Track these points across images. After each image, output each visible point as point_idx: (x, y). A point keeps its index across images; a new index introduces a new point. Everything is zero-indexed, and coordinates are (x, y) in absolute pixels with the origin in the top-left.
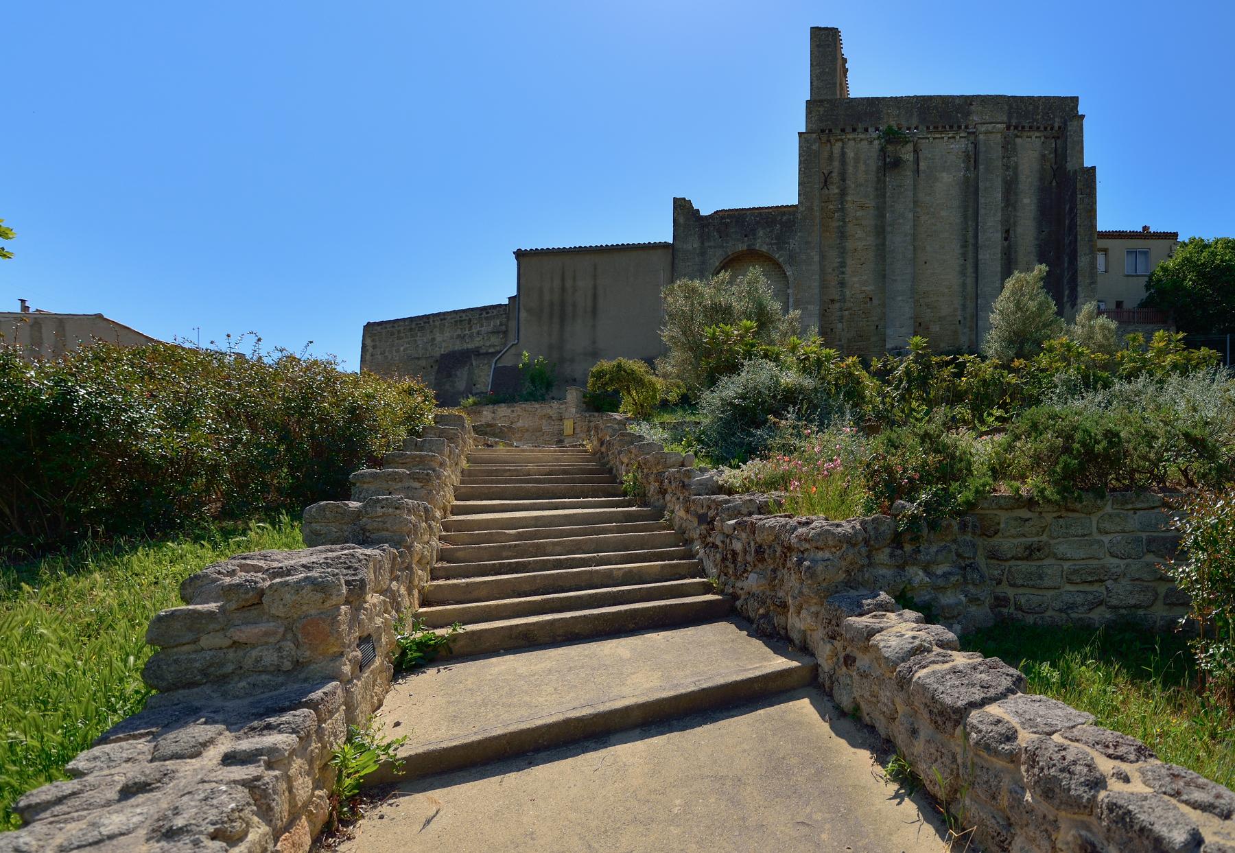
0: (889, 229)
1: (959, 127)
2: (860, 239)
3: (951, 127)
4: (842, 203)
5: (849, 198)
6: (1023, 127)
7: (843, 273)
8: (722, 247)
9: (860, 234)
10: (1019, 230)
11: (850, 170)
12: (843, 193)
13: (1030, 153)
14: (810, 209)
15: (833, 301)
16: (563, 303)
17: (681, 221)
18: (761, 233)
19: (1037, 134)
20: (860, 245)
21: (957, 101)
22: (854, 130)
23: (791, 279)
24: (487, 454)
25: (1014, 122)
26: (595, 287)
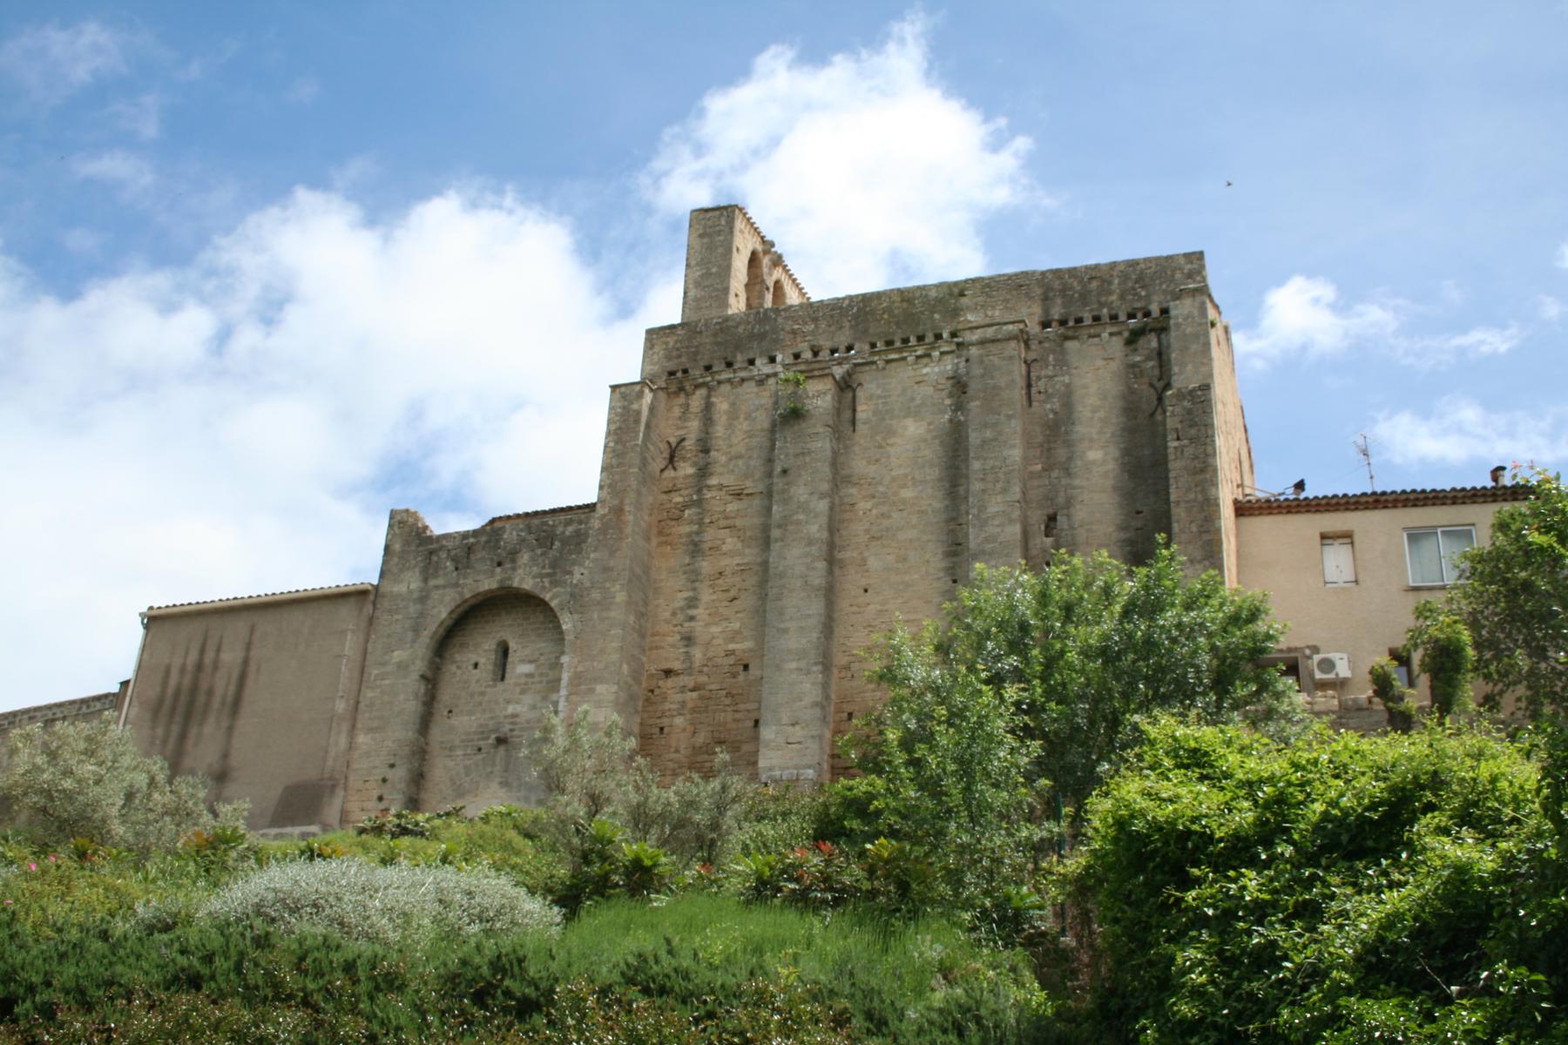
0: (775, 533)
1: (938, 337)
2: (731, 554)
3: (921, 339)
4: (699, 491)
5: (713, 481)
6: (1079, 320)
7: (692, 618)
8: (456, 585)
9: (731, 543)
10: (1080, 514)
11: (719, 430)
12: (703, 472)
13: (1096, 376)
14: (618, 511)
15: (668, 673)
16: (194, 689)
17: (397, 547)
18: (525, 558)
19: (1110, 329)
20: (729, 563)
21: (933, 294)
22: (729, 365)
23: (569, 637)
24: (216, 702)
25: (1056, 313)
26: (246, 662)
